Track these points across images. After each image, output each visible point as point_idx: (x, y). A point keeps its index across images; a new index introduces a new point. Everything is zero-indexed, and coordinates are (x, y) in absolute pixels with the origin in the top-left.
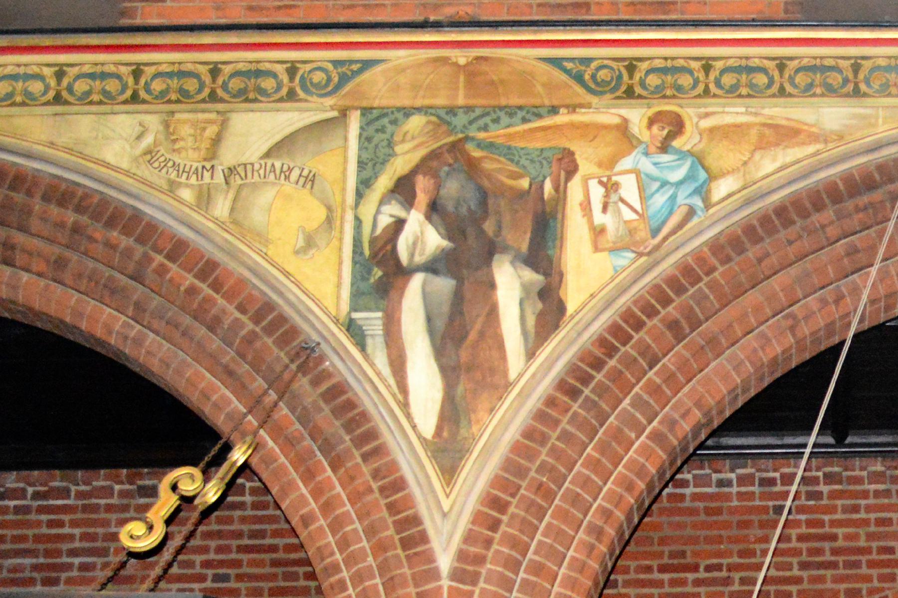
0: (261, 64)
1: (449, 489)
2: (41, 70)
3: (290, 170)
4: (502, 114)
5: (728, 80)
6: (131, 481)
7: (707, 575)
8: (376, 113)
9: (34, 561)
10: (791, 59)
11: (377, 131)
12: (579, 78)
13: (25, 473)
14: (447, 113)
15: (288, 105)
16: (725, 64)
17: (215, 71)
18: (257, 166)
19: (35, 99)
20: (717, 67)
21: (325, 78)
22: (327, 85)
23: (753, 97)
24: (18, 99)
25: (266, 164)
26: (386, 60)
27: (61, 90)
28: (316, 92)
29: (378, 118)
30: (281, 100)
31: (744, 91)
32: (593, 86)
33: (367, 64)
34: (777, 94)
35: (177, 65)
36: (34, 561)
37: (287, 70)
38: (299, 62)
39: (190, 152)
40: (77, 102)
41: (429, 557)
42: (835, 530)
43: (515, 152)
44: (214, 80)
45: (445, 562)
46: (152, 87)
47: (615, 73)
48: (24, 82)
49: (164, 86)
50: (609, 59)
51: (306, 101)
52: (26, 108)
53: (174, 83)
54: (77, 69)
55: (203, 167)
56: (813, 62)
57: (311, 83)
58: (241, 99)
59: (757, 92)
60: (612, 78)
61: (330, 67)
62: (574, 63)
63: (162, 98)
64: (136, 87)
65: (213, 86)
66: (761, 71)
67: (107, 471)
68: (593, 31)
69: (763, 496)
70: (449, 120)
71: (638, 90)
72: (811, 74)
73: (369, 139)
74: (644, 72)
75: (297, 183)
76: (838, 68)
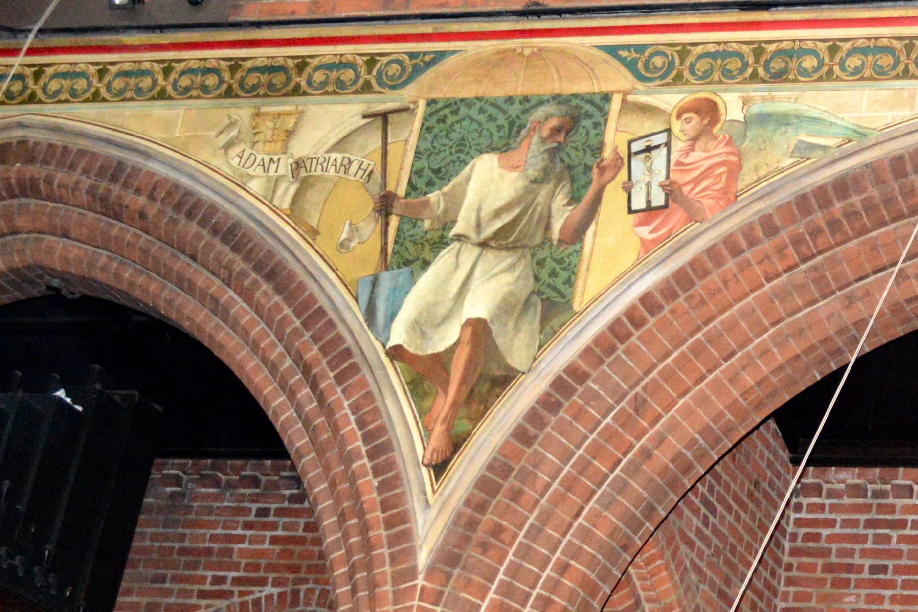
0: (729, 45)
2: (286, 61)
3: (350, 162)
5: (854, 62)
6: (236, 470)
7: (886, 562)
10: (179, 61)
11: (438, 121)
12: (631, 66)
15: (825, 84)
16: (853, 44)
17: (833, 49)
18: (321, 160)
20: (769, 50)
22: (401, 76)
32: (648, 75)
33: (440, 56)
35: (873, 40)
37: (367, 62)
41: (411, 553)
44: (832, 57)
45: (423, 559)
47: (668, 58)
49: (59, 86)
51: (380, 93)
55: (271, 159)
56: (867, 43)
57: (386, 74)
59: (879, 74)
60: (664, 63)
63: (185, 94)
66: (809, 54)
73: (429, 130)
76: (816, 52)
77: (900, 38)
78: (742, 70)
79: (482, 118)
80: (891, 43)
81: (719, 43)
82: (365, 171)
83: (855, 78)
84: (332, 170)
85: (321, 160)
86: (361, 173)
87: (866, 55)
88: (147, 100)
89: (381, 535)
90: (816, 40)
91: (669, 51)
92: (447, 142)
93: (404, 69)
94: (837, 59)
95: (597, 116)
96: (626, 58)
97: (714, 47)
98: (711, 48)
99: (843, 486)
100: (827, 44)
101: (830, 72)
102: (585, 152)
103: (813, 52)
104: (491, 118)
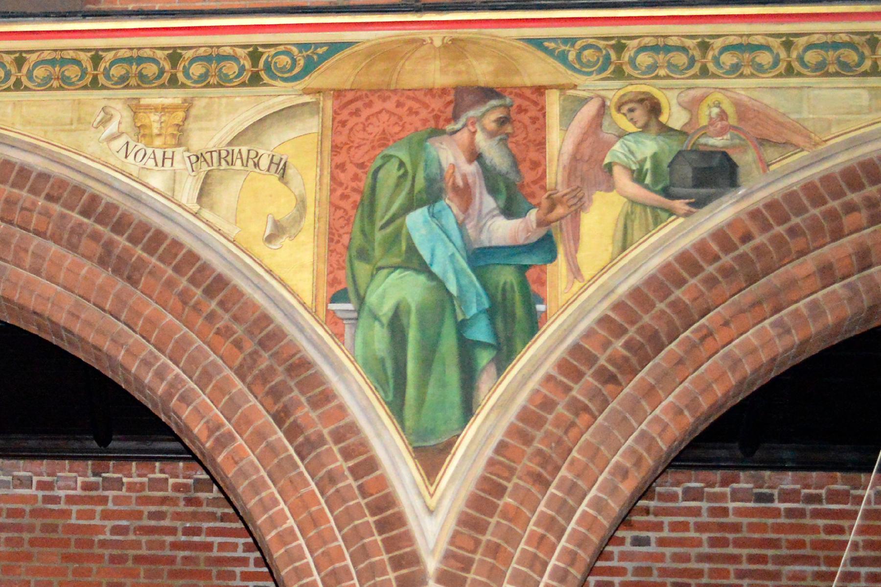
1: (434, 487)
4: (375, 98)
8: (350, 96)
9: (816, 568)
11: (351, 114)
12: (562, 58)
13: (802, 474)
14: (425, 95)
16: (116, 54)
17: (704, 46)
18: (224, 154)
19: (72, 84)
20: (631, 46)
21: (290, 62)
23: (222, 86)
24: (832, 69)
25: (233, 150)
26: (357, 43)
27: (97, 75)
28: (280, 75)
29: (351, 102)
30: (162, 86)
31: (213, 80)
32: (577, 66)
34: (12, 87)
35: (135, 51)
36: (816, 568)
37: (169, 56)
38: (180, 48)
39: (168, 138)
40: (193, 85)
42: (697, 535)
43: (389, 137)
46: (191, 72)
48: (61, 66)
50: (594, 38)
52: (62, 92)
53: (831, 55)
54: (805, 38)
58: (122, 86)
61: (295, 50)
62: (556, 43)
64: (95, 72)
65: (788, 59)
67: (818, 473)
68: (22, 23)
69: (722, 497)
70: (427, 102)
71: (102, 80)
72: (823, 52)
73: (343, 123)
74: (108, 64)
75: (268, 170)
77: (778, 35)
78: (776, 62)
79: (400, 111)
80: (682, 42)
81: (741, 36)
82: (278, 165)
83: (200, 85)
84: (239, 162)
85: (224, 154)
86: (274, 167)
87: (54, 66)
88: (773, 77)
89: (368, 522)
90: (235, 46)
91: (601, 44)
92: (366, 136)
93: (294, 62)
94: (25, 70)
95: (533, 112)
96: (554, 50)
97: (205, 51)
98: (47, 56)
99: (191, 481)
100: (13, 56)
101: (95, 79)
102: (527, 146)
103: (234, 58)
104: (411, 111)
